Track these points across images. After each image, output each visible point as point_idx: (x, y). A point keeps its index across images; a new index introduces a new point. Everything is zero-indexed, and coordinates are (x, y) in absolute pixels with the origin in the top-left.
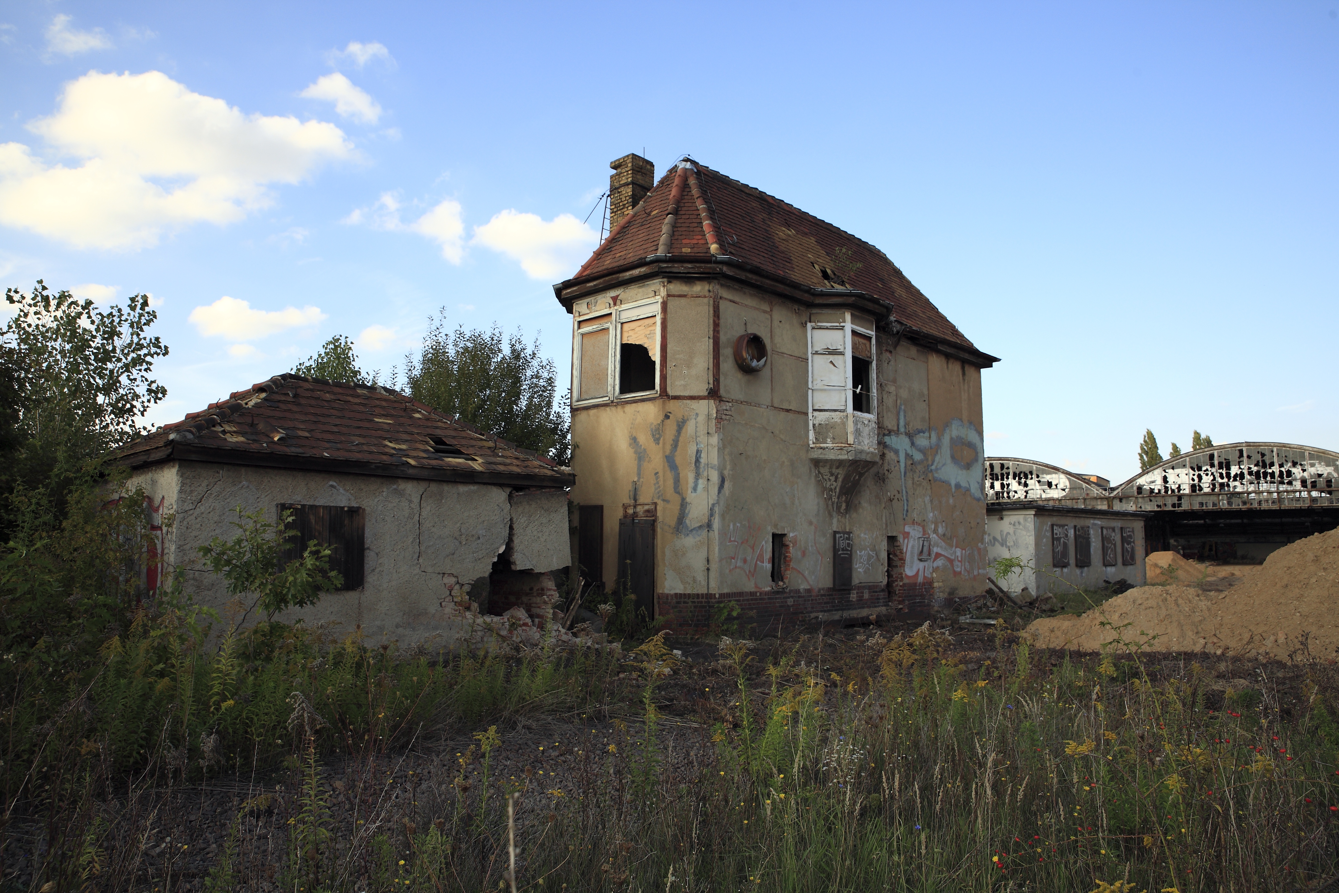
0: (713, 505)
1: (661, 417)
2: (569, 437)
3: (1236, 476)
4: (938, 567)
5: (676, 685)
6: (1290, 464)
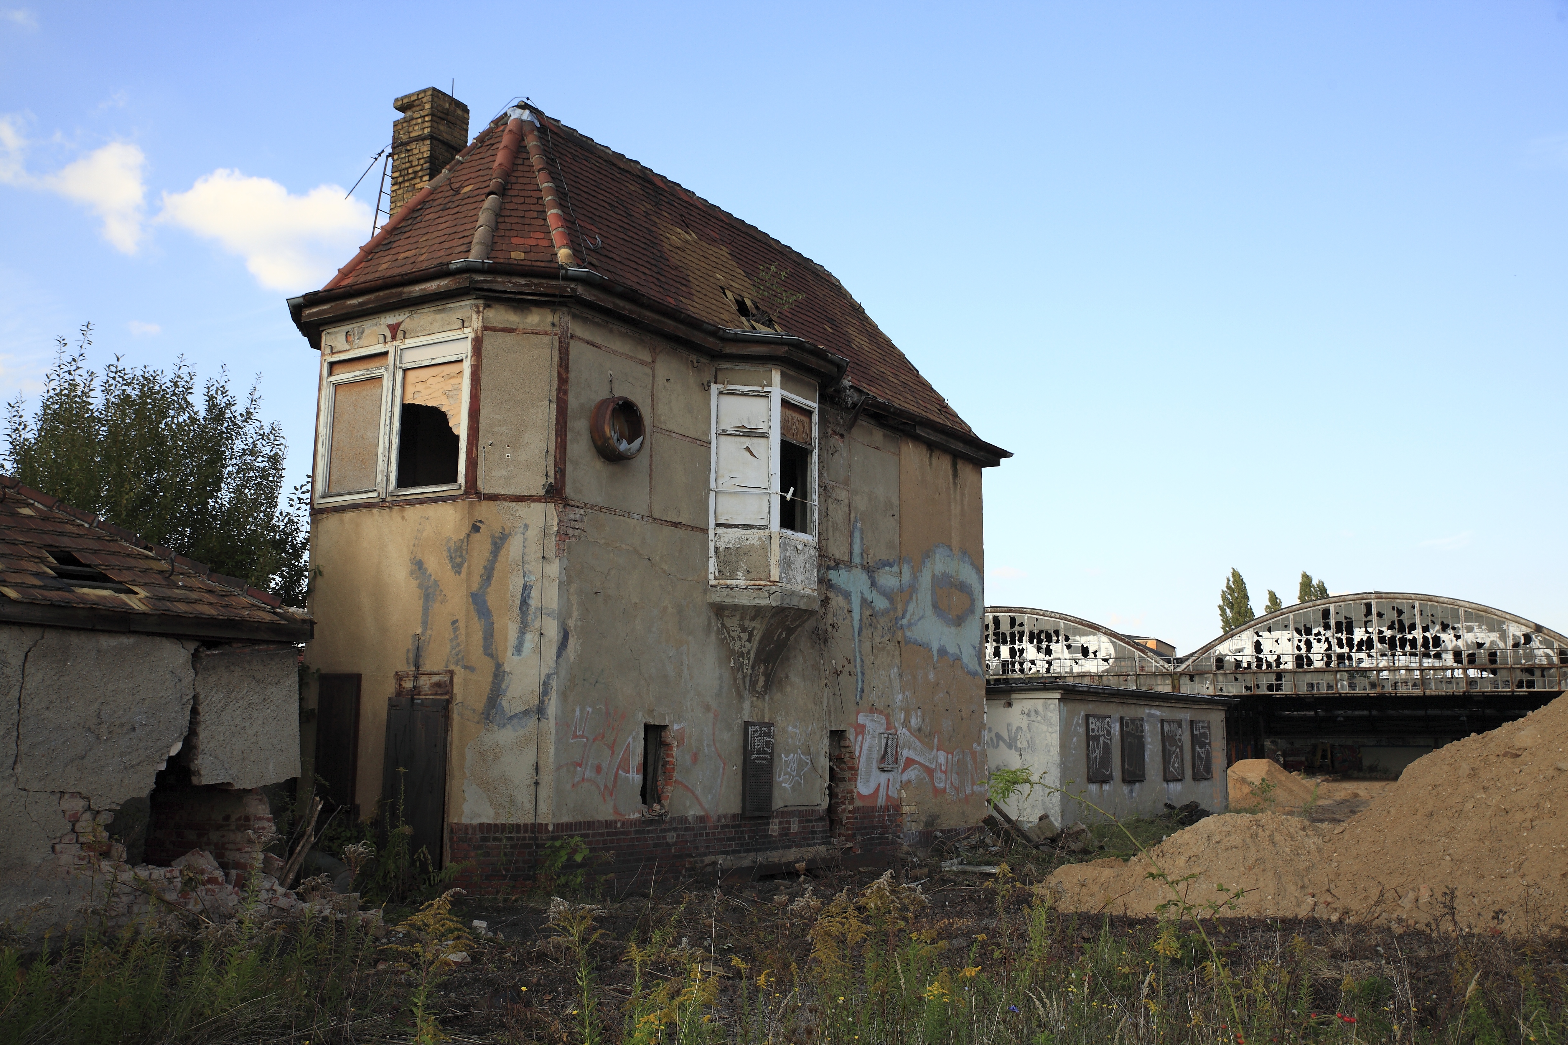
0: (548, 676)
1: (466, 529)
2: (306, 556)
4: (909, 781)
5: (476, 980)
6: (1438, 627)
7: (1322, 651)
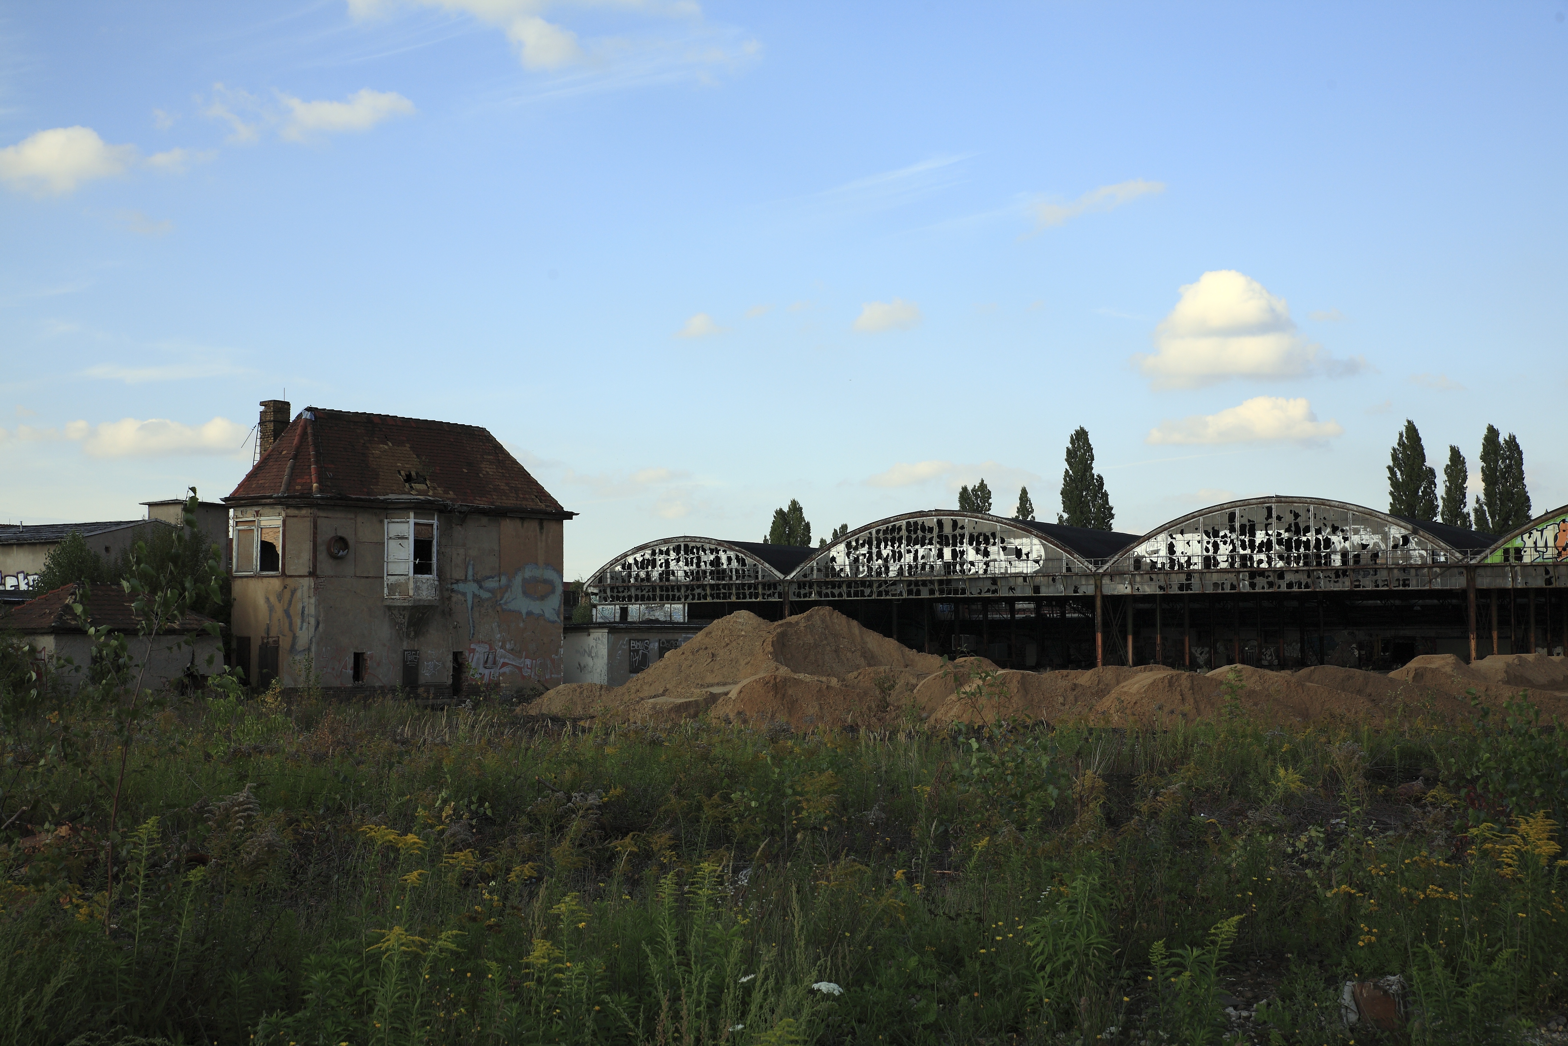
3: (1262, 544)
6: (1329, 530)
7: (1227, 552)
